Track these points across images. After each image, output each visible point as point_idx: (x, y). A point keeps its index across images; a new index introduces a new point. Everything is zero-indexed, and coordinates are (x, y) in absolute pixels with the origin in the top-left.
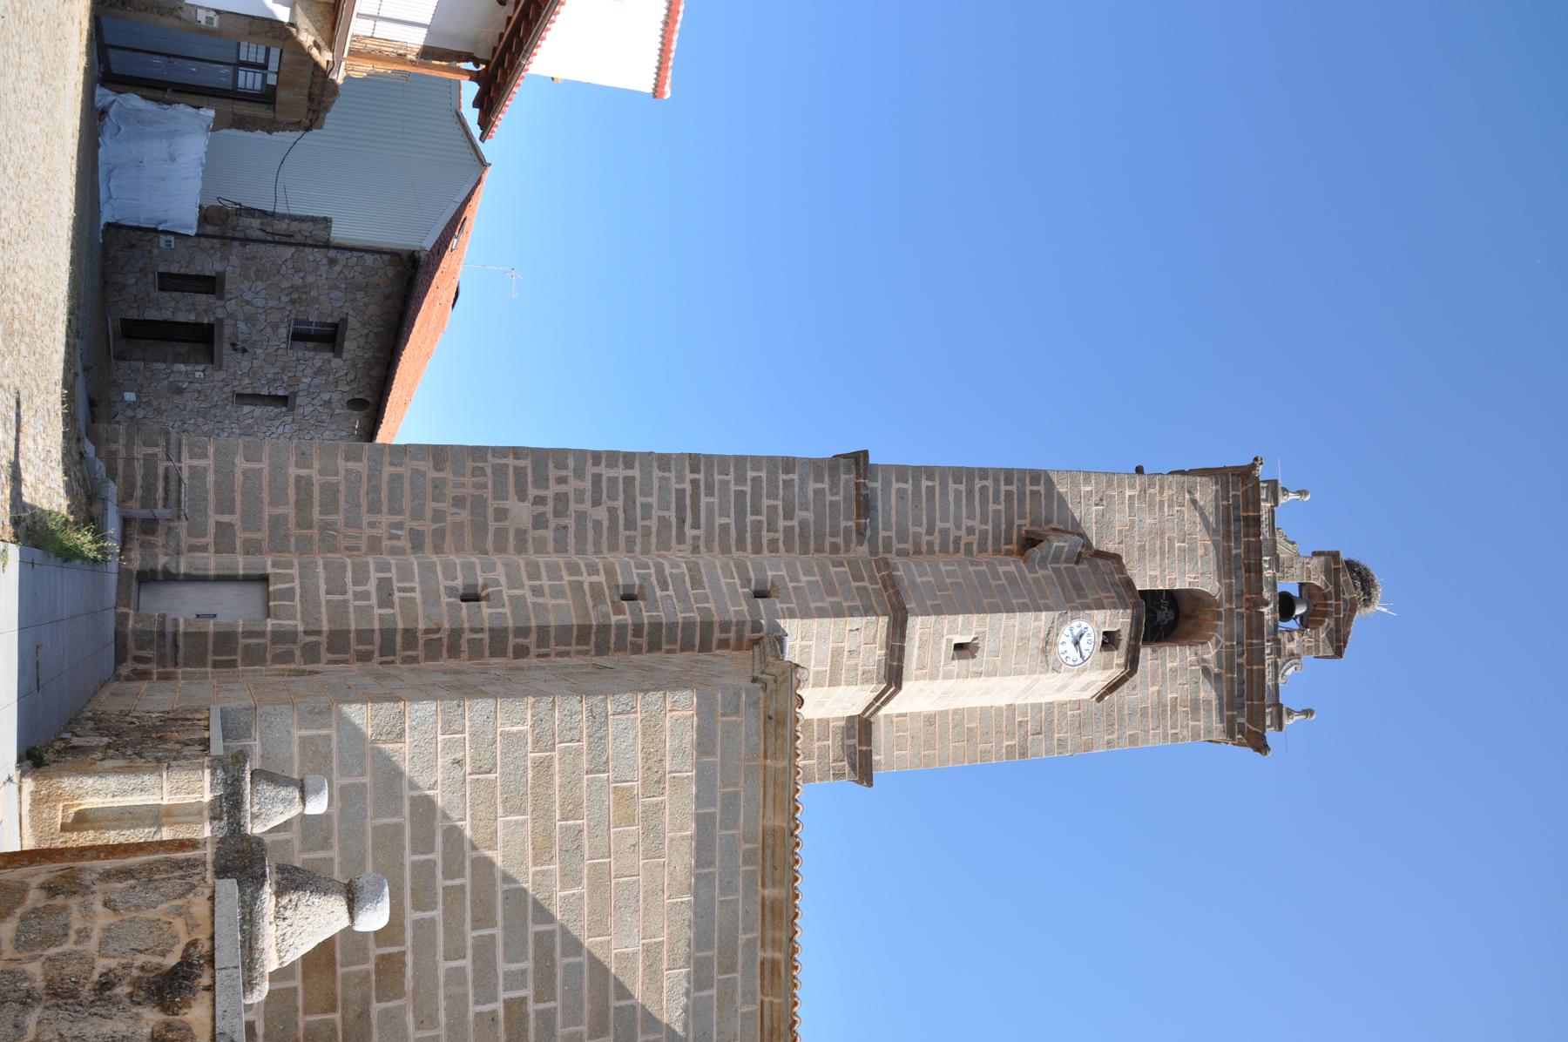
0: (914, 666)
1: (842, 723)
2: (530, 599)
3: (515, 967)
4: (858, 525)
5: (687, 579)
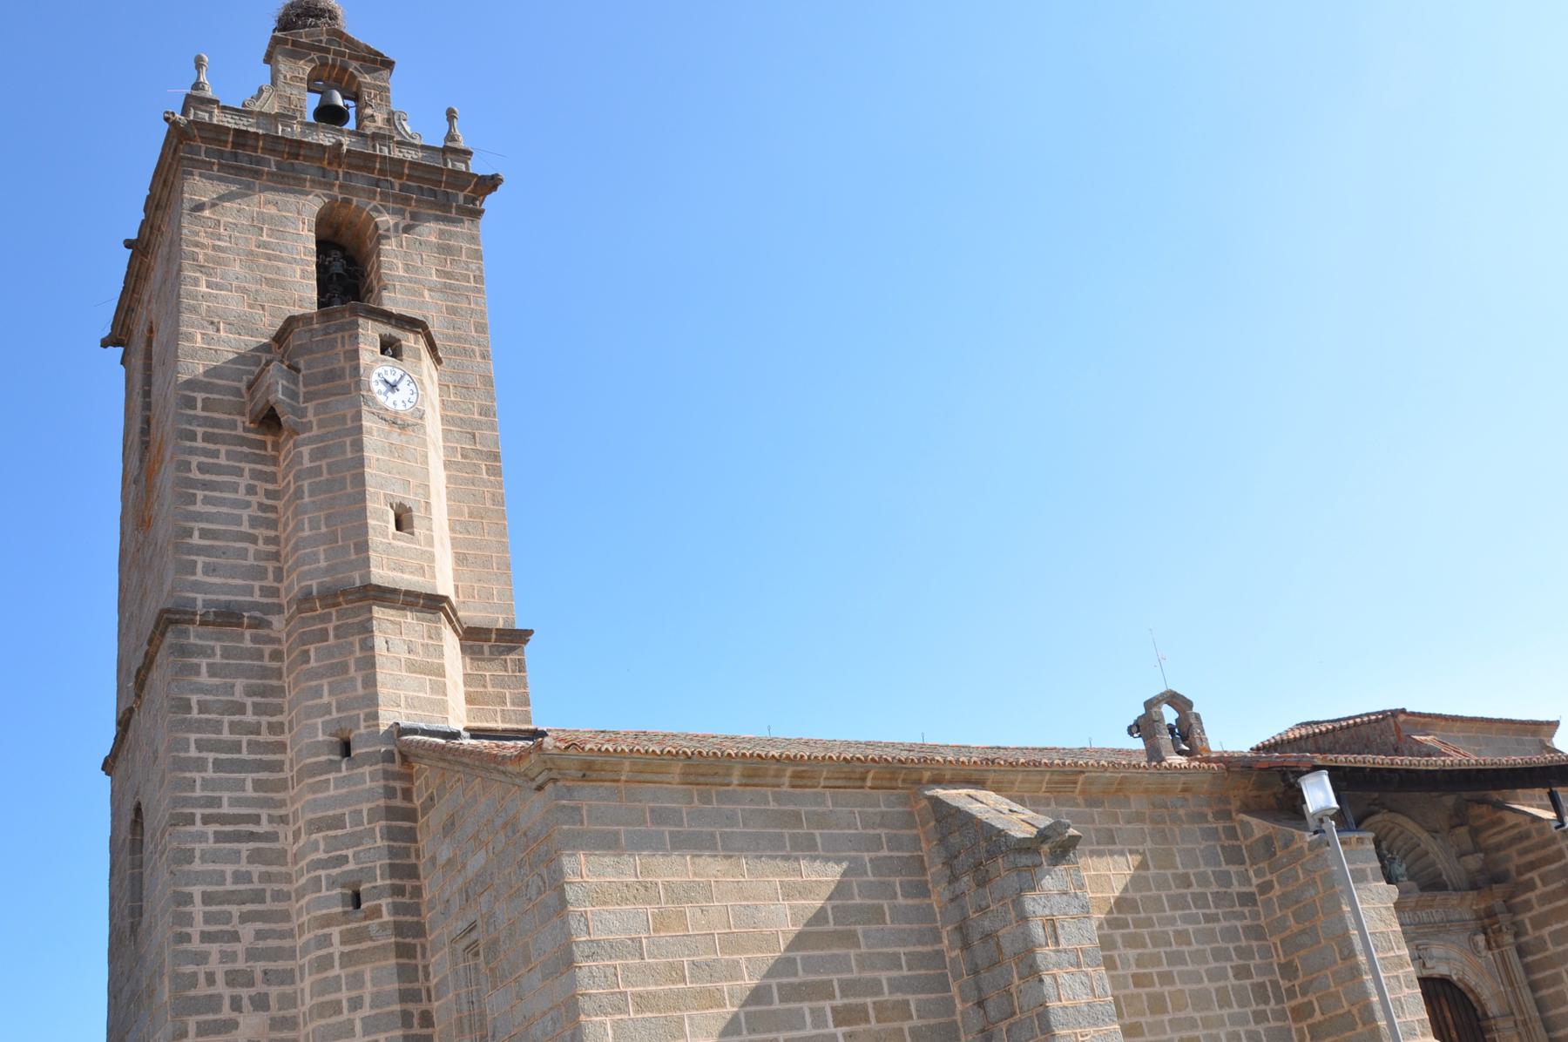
0: (420, 579)
1: (468, 660)
2: (366, 1011)
3: (808, 1019)
4: (249, 627)
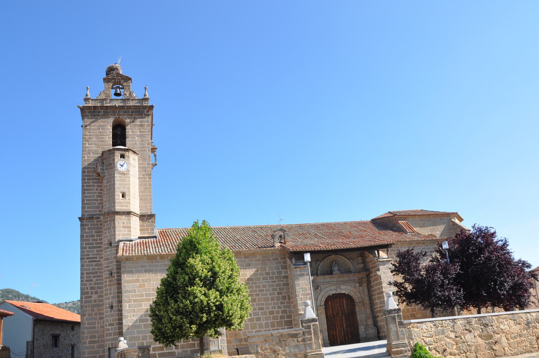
1: (141, 222)
2: (112, 295)
4: (96, 219)
5: (108, 261)
